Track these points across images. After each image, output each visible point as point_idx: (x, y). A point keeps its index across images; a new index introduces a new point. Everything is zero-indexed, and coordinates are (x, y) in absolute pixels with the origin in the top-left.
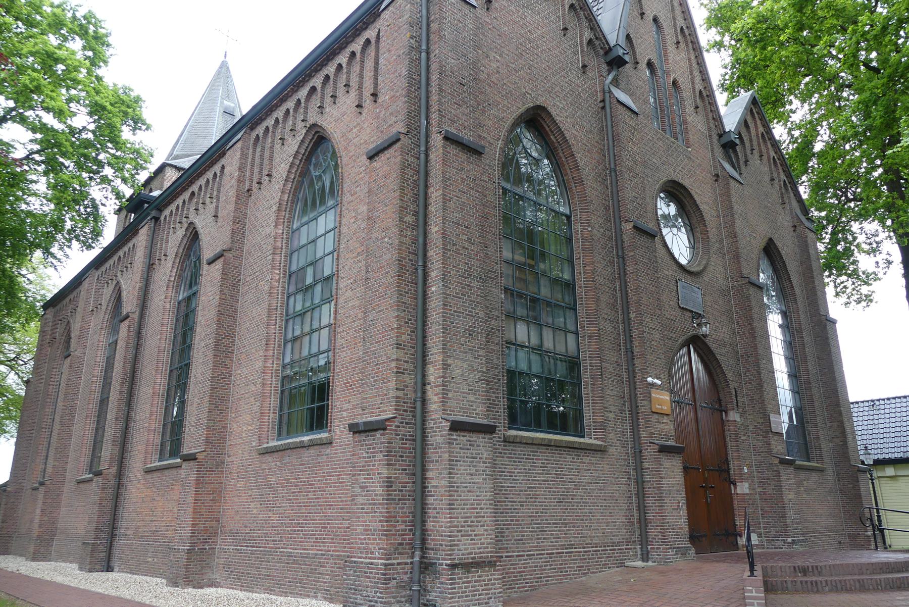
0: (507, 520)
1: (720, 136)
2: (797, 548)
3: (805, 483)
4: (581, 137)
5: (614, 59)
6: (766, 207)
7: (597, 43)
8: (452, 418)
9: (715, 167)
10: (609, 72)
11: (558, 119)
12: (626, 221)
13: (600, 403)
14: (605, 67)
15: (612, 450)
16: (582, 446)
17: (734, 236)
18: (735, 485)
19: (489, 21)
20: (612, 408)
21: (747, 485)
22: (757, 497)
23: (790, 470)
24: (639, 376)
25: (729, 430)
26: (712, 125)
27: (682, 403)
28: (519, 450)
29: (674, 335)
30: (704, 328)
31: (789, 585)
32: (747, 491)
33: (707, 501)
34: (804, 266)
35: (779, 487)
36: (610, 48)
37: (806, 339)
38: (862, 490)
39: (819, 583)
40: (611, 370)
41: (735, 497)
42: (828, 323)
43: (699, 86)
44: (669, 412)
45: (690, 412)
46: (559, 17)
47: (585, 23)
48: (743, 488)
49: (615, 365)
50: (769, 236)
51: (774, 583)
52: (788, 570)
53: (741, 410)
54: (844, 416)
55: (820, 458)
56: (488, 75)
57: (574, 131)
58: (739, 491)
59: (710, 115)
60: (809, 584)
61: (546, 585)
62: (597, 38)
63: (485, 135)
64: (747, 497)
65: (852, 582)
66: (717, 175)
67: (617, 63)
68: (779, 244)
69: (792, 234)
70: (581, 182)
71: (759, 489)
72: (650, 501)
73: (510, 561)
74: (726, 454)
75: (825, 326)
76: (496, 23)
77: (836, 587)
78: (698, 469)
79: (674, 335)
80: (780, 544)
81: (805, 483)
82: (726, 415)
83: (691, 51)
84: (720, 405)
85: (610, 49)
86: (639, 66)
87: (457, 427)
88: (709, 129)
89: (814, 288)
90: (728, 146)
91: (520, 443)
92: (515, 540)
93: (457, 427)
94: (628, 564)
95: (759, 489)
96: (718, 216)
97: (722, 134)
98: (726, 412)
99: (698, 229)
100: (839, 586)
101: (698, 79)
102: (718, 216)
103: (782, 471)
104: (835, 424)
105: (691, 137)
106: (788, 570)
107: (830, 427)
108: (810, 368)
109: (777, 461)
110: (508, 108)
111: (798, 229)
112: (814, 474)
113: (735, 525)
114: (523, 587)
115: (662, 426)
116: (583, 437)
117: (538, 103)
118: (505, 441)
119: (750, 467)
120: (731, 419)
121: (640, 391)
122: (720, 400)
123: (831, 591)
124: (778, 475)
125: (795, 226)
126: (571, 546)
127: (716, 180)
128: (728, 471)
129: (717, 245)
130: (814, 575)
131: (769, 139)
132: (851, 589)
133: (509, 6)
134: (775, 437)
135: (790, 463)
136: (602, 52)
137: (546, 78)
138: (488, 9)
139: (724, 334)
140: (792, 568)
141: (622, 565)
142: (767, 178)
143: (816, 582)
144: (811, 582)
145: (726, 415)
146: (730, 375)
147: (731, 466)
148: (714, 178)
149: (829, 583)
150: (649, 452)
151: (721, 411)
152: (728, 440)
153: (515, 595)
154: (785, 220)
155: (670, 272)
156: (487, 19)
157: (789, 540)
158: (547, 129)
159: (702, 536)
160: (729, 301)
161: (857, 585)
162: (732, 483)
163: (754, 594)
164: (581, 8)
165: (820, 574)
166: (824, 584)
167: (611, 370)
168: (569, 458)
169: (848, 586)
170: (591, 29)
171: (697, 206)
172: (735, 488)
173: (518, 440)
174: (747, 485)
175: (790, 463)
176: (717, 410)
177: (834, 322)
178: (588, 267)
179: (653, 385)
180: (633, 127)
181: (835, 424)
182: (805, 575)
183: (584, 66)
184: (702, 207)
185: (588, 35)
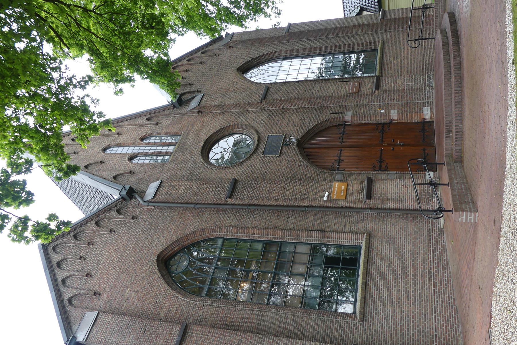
0: (413, 325)
1: (174, 107)
2: (433, 84)
3: (391, 59)
4: (175, 227)
5: (128, 196)
6: (218, 70)
7: (119, 206)
8: (365, 198)
9: (193, 113)
10: (136, 198)
11: (166, 245)
12: (227, 201)
13: (337, 236)
14: (133, 201)
15: (369, 229)
16: (367, 255)
17: (235, 105)
18: (392, 120)
19: (107, 294)
20: (343, 224)
21: (392, 111)
22: (400, 103)
23: (383, 80)
24: (323, 204)
25: (357, 120)
26: (168, 113)
27: (340, 159)
28: (369, 309)
29: (297, 163)
30: (293, 140)
31: (458, 148)
32: (396, 111)
33: (402, 146)
34: (254, 43)
35: (394, 91)
36: (122, 198)
37: (300, 47)
38: (396, 17)
39: (457, 130)
40: (318, 221)
41: (400, 121)
42: (290, 31)
43: (144, 120)
44: (345, 184)
45: (346, 153)
46: (104, 234)
47: (107, 214)
48: (394, 115)
49: (316, 218)
50: (236, 71)
51: (457, 157)
52: (448, 141)
53: (345, 111)
54: (348, 24)
55: (376, 43)
56: (139, 300)
57: (172, 232)
58: (396, 118)
59: (162, 113)
60: (457, 136)
61: (454, 299)
62: (116, 206)
63: (175, 308)
64: (400, 111)
65: (457, 109)
66: (199, 112)
67: (131, 194)
68: (239, 66)
69: (234, 49)
70: (202, 231)
71: (395, 101)
72: (402, 206)
73: (438, 330)
74: (372, 124)
75: (292, 33)
76: (107, 289)
77: (459, 120)
78: (382, 150)
79: (297, 163)
80: (430, 94)
81: (391, 59)
82: (348, 122)
83: (123, 123)
84: (342, 125)
85: (122, 198)
86: (132, 169)
87: (369, 196)
88: (170, 114)
89: (268, 38)
90: (180, 102)
91: (364, 308)
92: (425, 321)
93: (369, 196)
94: (442, 227)
95: (395, 101)
96: (223, 113)
97: (173, 106)
98: (346, 122)
99: (231, 131)
100: (459, 118)
101: (139, 120)
102: (223, 113)
103: (384, 88)
104: (354, 30)
105: (175, 130)
106: (448, 141)
107: (356, 32)
108: (318, 45)
109: (377, 92)
110: (158, 286)
111: (231, 45)
112: (385, 50)
113: (417, 123)
114: (455, 319)
115: (354, 191)
116: (361, 247)
117: (155, 261)
118: (363, 321)
119: (381, 107)
120: (350, 119)
121: (332, 205)
122: (339, 125)
123: (462, 123)
124: (386, 91)
125: (230, 47)
126: (430, 272)
127: (202, 112)
128: (383, 124)
129: (241, 117)
130: (451, 126)
131: (176, 63)
132: (461, 111)
133: (97, 276)
134: (362, 89)
135: (378, 79)
136: (124, 202)
137: (140, 252)
138: (99, 295)
139: (296, 118)
140: (448, 138)
141: (442, 230)
142: (200, 67)
143: (456, 132)
144: (456, 135)
145: (348, 122)
146: (322, 118)
147: (380, 121)
148: (200, 113)
149: (457, 124)
150: (370, 204)
151: (345, 125)
152: (363, 122)
153: (460, 327)
154: (226, 55)
155: (258, 160)
156: (105, 296)
157: (428, 88)
158: (171, 252)
159: (425, 153)
160: (276, 111)
161: (458, 106)
162: (390, 122)
163: (464, 217)
164: (98, 217)
165: (451, 122)
166: (458, 127)
167: (318, 221)
168: (374, 266)
169: (460, 112)
170: (110, 210)
171: (217, 131)
172: (394, 120)
173: (362, 310)
174: (392, 111)
175: (378, 79)
176: (344, 127)
177: (290, 25)
178: (255, 232)
179: (328, 196)
180: (169, 187)
181: (354, 30)
182: (451, 131)
183: (133, 218)
184: (218, 128)
185: (114, 213)
